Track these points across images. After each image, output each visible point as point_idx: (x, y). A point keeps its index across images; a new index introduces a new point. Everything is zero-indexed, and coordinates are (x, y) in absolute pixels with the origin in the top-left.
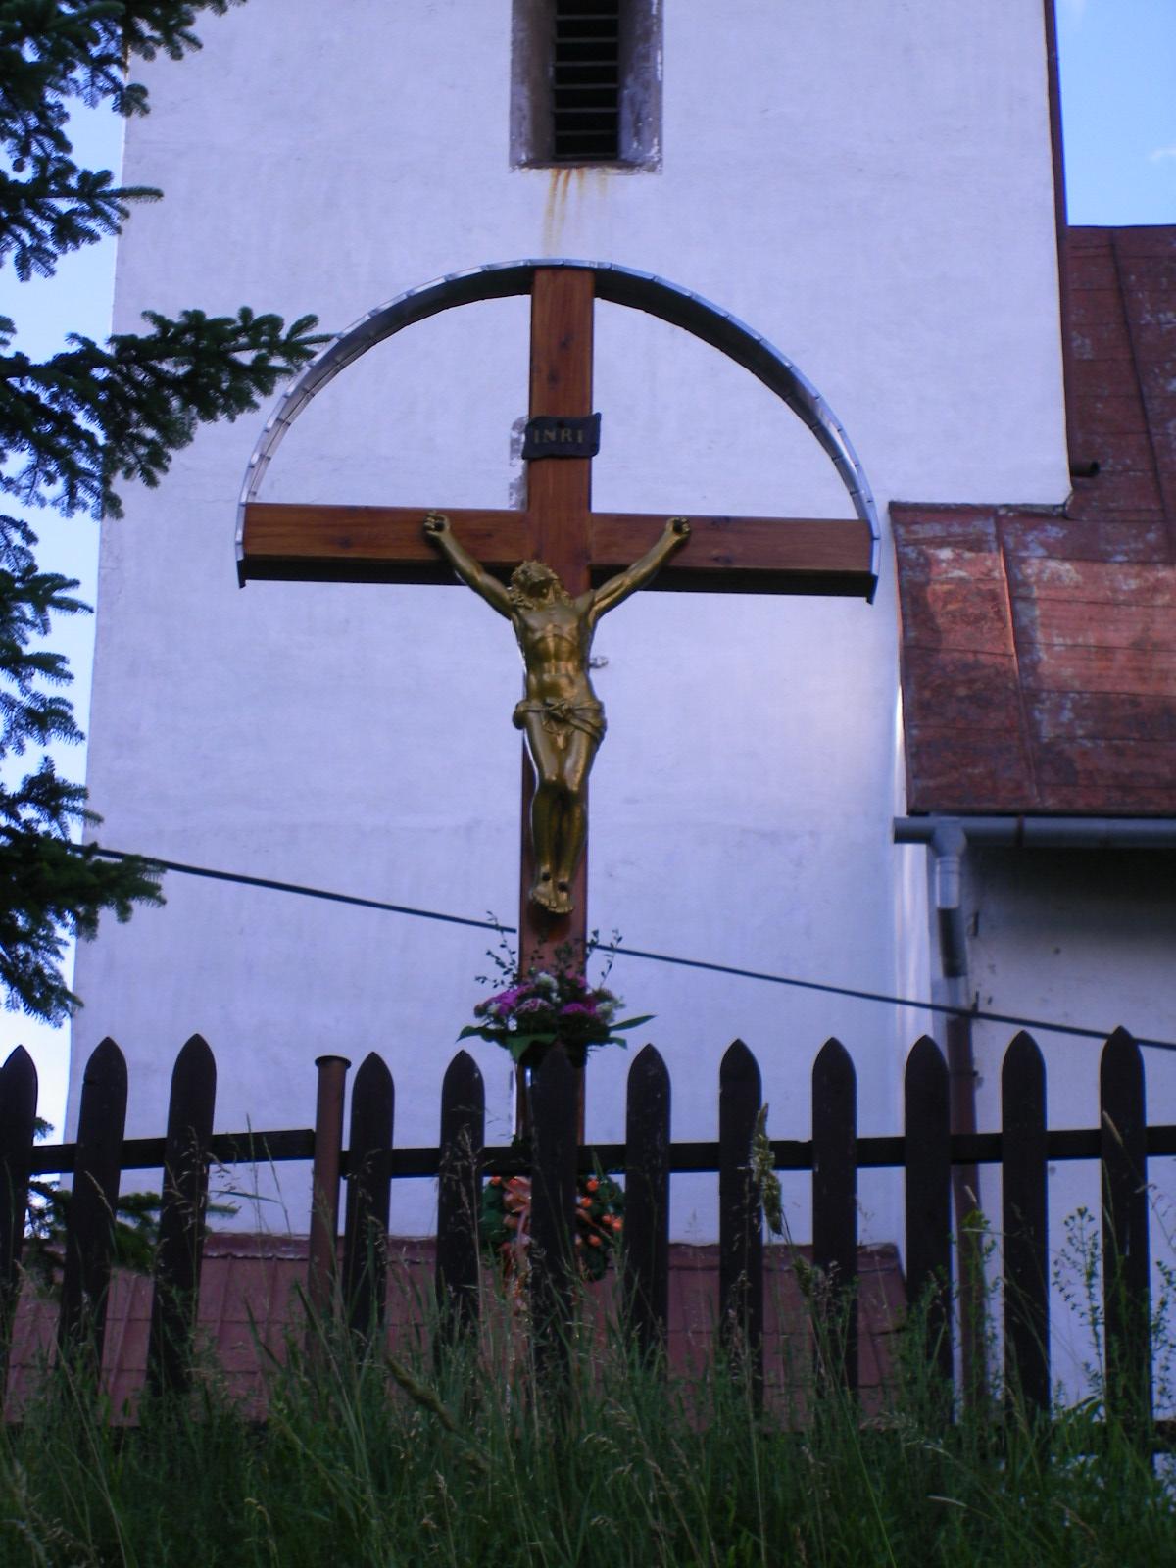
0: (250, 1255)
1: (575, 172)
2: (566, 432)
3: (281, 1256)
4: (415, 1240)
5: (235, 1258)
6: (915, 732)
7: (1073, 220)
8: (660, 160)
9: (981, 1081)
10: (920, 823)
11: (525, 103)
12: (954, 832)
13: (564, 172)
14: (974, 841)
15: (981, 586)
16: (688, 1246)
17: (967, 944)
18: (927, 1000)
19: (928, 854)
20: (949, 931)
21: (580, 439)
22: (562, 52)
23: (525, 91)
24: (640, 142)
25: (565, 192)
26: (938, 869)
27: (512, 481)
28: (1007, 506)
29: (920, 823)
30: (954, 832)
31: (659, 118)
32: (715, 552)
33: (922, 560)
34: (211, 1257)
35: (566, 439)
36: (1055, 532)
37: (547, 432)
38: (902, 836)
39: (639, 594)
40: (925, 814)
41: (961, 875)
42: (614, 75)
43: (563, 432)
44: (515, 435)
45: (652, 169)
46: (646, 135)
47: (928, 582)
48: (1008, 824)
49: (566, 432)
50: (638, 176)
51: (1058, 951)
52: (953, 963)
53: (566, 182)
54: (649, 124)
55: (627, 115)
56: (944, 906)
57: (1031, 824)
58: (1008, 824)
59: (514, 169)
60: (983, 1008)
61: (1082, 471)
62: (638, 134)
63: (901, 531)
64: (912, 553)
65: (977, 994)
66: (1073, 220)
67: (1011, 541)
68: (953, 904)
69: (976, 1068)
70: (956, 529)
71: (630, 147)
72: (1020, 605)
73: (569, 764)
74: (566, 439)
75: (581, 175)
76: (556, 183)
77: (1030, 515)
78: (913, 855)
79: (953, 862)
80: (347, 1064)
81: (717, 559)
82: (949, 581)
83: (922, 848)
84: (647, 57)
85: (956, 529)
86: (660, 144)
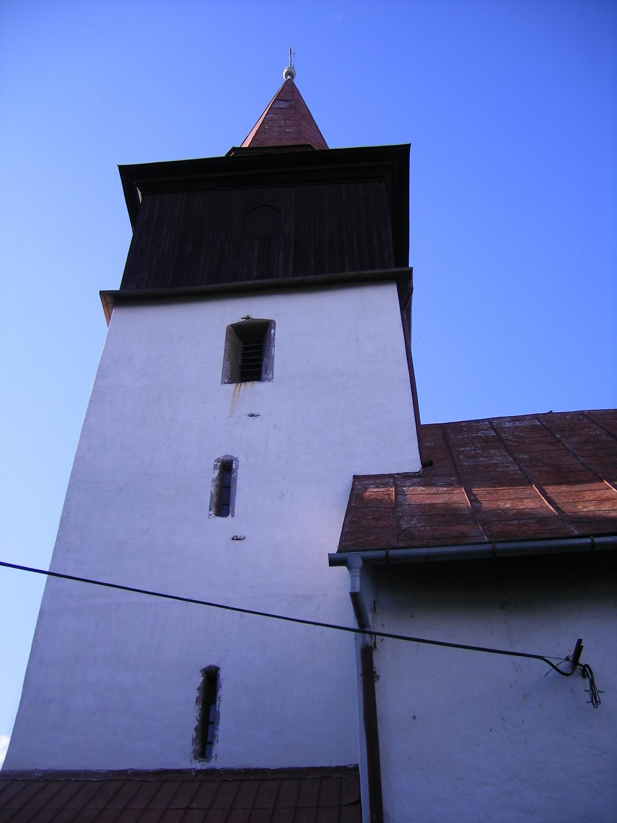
0: (77, 779)
1: (243, 383)
4: (150, 771)
5: (71, 781)
7: (423, 422)
8: (273, 378)
9: (378, 677)
10: (342, 555)
11: (228, 367)
12: (357, 559)
13: (239, 384)
14: (366, 561)
16: (268, 769)
17: (370, 616)
22: (244, 355)
23: (228, 363)
25: (240, 389)
29: (342, 555)
31: (273, 366)
34: (61, 781)
41: (361, 577)
42: (261, 360)
45: (270, 381)
46: (268, 372)
48: (383, 553)
50: (265, 383)
51: (413, 616)
52: (375, 643)
53: (241, 385)
55: (264, 368)
56: (353, 591)
58: (383, 553)
59: (222, 384)
66: (423, 422)
68: (358, 590)
71: (264, 376)
76: (237, 387)
77: (406, 476)
79: (357, 572)
80: (356, 768)
83: (344, 568)
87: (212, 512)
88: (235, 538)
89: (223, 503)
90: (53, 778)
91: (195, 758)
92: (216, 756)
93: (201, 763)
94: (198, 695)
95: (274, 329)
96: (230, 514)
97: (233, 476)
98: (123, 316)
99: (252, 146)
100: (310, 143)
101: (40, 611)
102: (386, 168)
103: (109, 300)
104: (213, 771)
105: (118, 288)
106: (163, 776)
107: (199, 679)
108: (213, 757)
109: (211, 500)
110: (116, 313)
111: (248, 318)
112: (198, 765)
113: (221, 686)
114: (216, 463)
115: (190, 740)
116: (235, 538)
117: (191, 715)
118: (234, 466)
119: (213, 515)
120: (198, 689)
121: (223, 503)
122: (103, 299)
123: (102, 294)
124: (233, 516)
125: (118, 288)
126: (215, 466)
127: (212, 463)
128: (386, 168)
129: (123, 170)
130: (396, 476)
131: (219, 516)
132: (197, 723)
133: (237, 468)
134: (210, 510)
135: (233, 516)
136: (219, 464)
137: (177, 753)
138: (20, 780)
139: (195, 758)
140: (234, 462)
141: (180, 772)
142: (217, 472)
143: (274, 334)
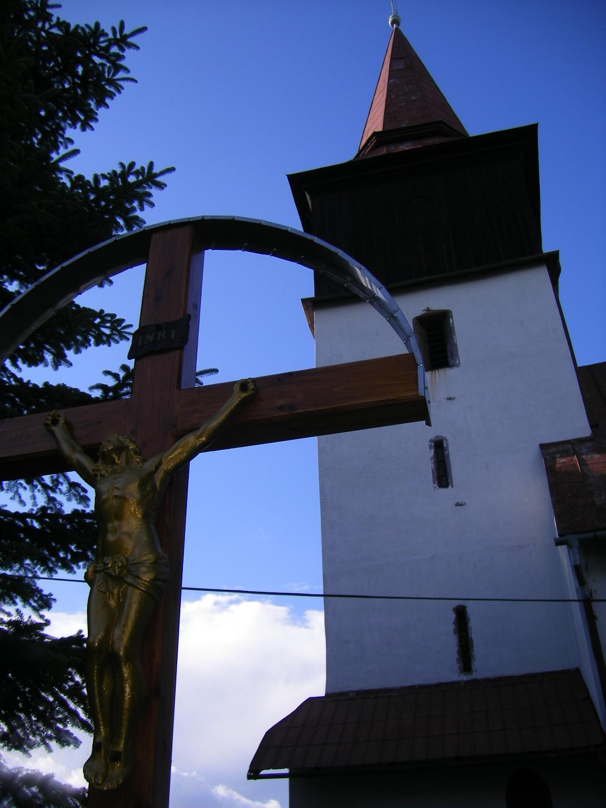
1: (437, 371)
2: (162, 333)
3: (392, 695)
6: (557, 510)
8: (460, 363)
10: (563, 538)
12: (574, 539)
13: (434, 372)
15: (570, 463)
17: (585, 574)
18: (576, 598)
19: (568, 548)
20: (578, 571)
21: (173, 336)
24: (453, 360)
26: (571, 552)
27: (431, 456)
28: (574, 440)
29: (563, 538)
30: (574, 539)
31: (457, 353)
32: (280, 402)
33: (552, 458)
35: (162, 337)
36: (589, 444)
37: (148, 336)
38: (558, 543)
39: (201, 456)
40: (564, 535)
43: (159, 333)
44: (430, 444)
45: (458, 366)
47: (555, 464)
48: (591, 535)
49: (162, 333)
52: (581, 581)
54: (455, 354)
55: (449, 354)
57: (599, 533)
58: (591, 535)
60: (595, 597)
61: (593, 426)
62: (453, 358)
63: (544, 451)
64: (548, 457)
65: (591, 590)
66: (579, 365)
67: (577, 449)
68: (578, 563)
69: (595, 614)
70: (560, 448)
72: (583, 467)
73: (117, 632)
74: (162, 337)
75: (439, 372)
78: (563, 550)
81: (281, 408)
82: (560, 463)
83: (566, 546)
84: (452, 338)
85: (560, 448)
86: (459, 359)
87: (435, 485)
88: (458, 505)
89: (443, 476)
90: (364, 695)
91: (461, 672)
92: (476, 670)
93: (466, 676)
94: (454, 628)
95: (452, 318)
96: (450, 485)
97: (446, 453)
98: (323, 317)
99: (387, 128)
100: (442, 119)
101: (324, 576)
102: (518, 148)
103: (309, 304)
104: (475, 681)
105: (313, 296)
106: (440, 686)
107: (452, 616)
108: (473, 671)
109: (433, 475)
110: (317, 315)
111: (428, 310)
112: (465, 677)
113: (469, 620)
114: (430, 444)
115: (455, 661)
116: (458, 505)
117: (452, 643)
118: (445, 445)
119: (437, 487)
120: (453, 623)
121: (443, 476)
122: (304, 305)
123: (303, 300)
124: (452, 486)
125: (313, 296)
126: (430, 446)
127: (427, 444)
128: (518, 148)
129: (291, 177)
130: (572, 442)
131: (442, 488)
132: (457, 648)
133: (447, 445)
134: (434, 483)
135: (452, 486)
136: (433, 444)
137: (447, 670)
138: (343, 700)
139: (461, 672)
140: (444, 442)
141: (452, 683)
142: (433, 451)
143: (453, 323)
